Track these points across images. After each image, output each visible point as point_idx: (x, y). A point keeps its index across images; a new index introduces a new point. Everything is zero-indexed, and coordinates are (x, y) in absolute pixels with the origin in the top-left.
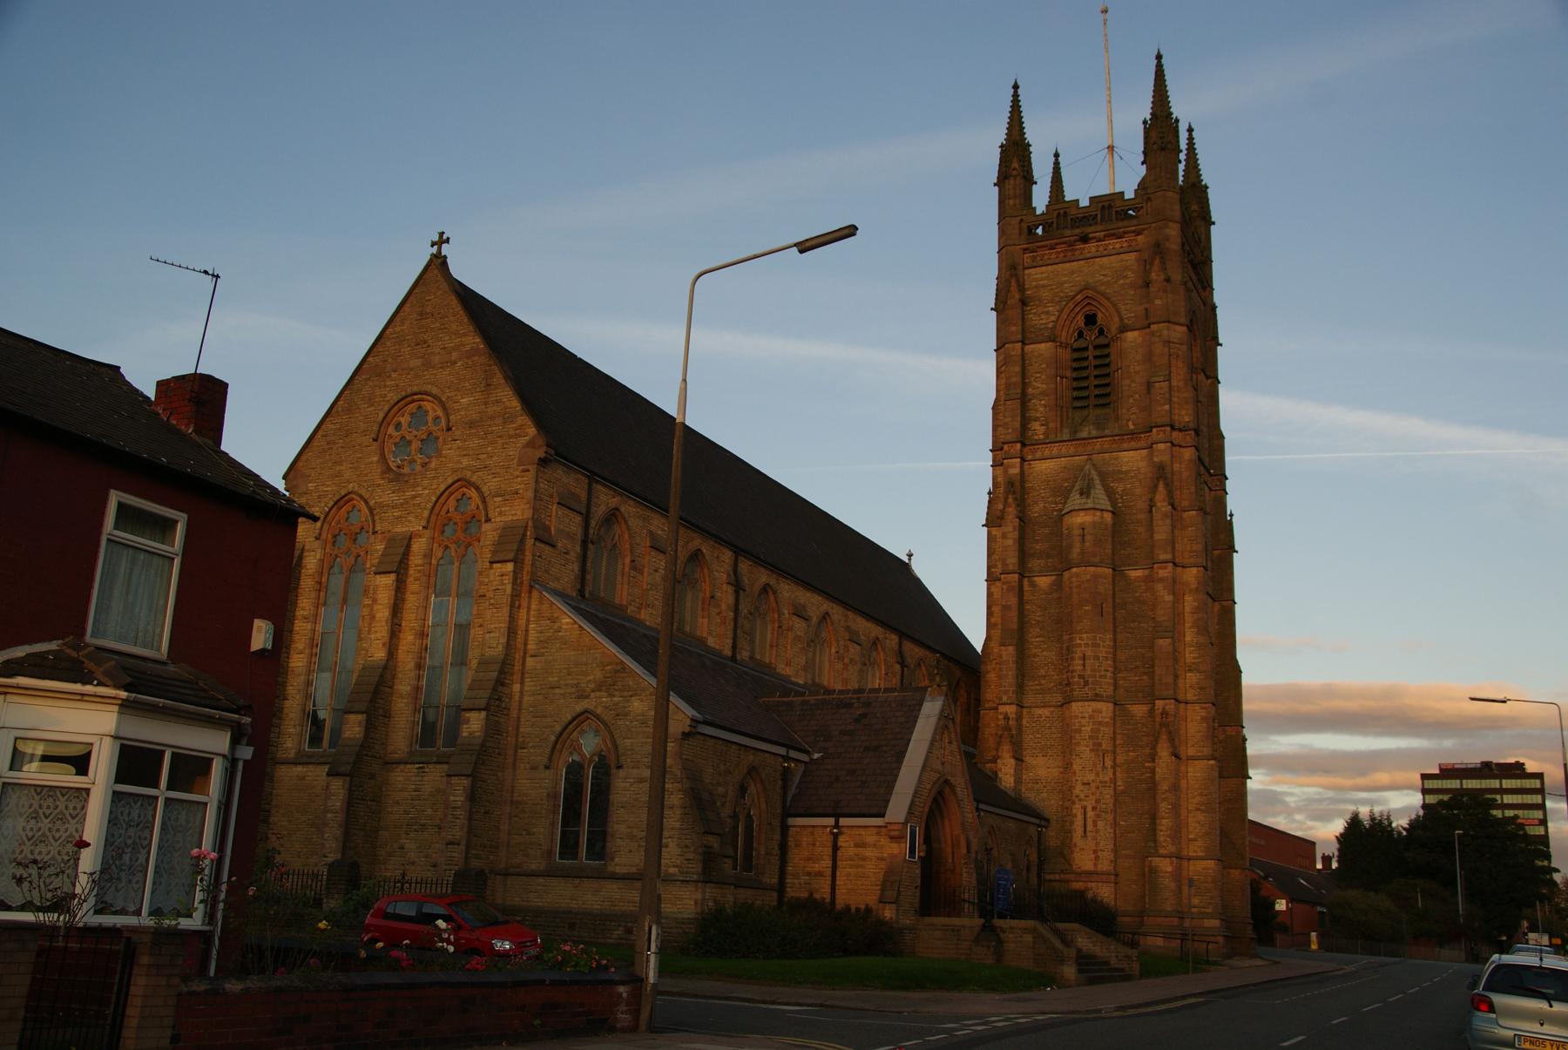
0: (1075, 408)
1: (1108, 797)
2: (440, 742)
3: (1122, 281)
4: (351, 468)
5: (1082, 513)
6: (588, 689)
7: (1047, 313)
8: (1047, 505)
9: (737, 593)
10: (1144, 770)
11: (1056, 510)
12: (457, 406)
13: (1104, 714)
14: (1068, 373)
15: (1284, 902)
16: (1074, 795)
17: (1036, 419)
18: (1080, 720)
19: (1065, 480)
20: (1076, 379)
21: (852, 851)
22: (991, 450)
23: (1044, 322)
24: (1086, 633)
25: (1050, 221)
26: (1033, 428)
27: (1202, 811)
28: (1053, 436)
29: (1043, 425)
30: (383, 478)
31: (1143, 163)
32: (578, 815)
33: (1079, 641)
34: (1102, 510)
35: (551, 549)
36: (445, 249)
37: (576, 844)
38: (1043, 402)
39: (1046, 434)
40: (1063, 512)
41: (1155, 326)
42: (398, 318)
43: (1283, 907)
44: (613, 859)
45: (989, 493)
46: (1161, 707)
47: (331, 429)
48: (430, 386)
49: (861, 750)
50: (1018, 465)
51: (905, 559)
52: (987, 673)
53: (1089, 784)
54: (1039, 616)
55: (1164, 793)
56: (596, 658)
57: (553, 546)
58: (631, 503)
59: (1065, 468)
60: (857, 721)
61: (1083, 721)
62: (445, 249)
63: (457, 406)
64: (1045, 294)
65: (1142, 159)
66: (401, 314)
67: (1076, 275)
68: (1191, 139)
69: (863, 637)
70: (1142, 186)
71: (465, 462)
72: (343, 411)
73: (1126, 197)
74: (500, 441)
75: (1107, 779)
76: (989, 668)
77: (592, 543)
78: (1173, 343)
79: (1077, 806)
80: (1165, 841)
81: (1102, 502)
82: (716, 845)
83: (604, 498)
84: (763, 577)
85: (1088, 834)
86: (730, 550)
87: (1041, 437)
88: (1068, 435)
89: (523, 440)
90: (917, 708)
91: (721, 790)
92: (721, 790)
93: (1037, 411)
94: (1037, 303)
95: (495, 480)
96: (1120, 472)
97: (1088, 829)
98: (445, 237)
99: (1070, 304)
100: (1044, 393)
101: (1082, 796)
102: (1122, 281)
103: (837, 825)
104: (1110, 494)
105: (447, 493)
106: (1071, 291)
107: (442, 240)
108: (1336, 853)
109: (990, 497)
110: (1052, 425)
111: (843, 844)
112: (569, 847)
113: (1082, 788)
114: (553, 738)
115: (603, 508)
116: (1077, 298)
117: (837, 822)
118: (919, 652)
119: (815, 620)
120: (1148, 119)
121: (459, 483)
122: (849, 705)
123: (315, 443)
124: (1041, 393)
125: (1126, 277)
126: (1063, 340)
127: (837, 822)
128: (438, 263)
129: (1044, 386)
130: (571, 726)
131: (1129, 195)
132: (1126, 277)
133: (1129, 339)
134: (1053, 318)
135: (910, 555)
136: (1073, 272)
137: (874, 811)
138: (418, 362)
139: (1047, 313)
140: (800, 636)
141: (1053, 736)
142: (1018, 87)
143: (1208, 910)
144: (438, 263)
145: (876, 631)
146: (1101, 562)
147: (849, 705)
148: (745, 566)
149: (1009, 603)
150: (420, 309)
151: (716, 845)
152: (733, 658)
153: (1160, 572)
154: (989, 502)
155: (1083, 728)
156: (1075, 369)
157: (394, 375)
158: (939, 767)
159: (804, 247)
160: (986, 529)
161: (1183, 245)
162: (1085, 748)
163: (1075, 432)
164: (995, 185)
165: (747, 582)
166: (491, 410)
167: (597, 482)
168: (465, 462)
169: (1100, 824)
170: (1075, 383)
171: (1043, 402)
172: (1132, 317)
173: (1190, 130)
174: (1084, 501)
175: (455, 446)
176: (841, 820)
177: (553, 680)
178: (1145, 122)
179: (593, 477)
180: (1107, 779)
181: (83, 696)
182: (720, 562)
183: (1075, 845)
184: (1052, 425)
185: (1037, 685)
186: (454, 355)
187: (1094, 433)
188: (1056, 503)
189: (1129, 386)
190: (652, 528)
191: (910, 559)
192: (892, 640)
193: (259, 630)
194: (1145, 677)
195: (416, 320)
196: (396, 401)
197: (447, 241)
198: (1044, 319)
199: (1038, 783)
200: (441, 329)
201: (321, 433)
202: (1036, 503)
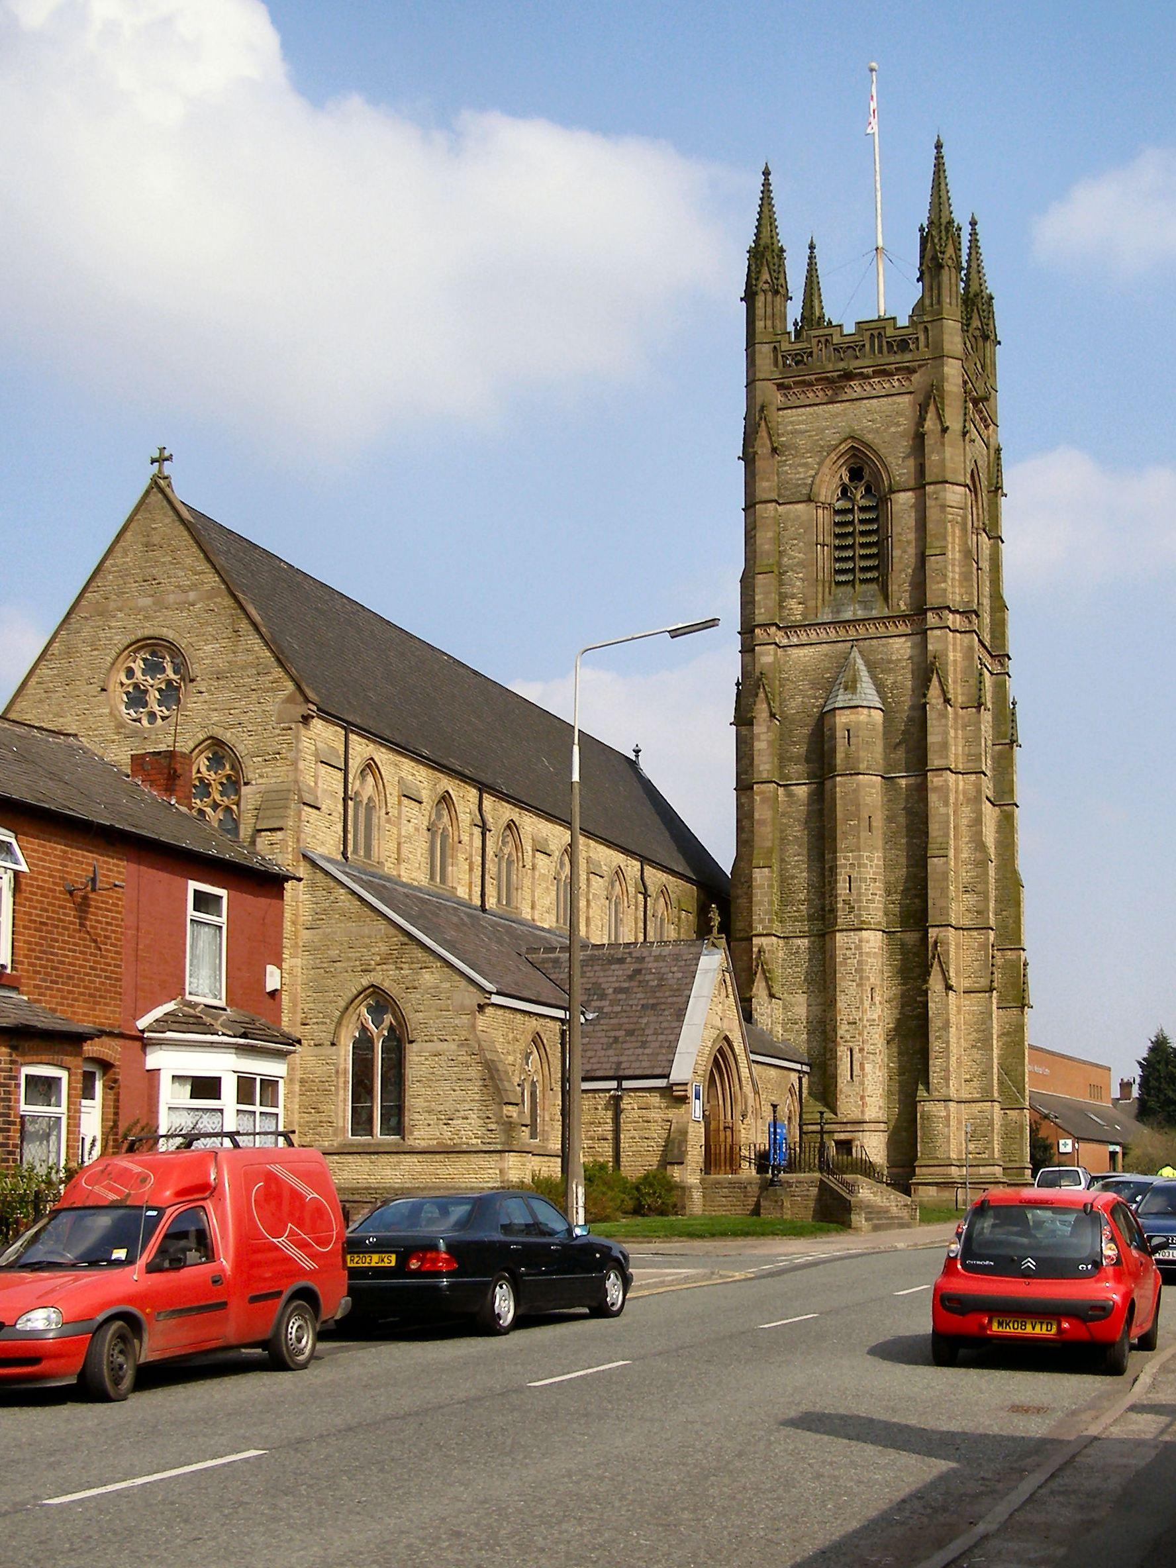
0: (838, 583)
1: (877, 1036)
2: (219, 1022)
3: (893, 429)
4: (77, 721)
5: (847, 712)
6: (373, 962)
7: (805, 465)
8: (806, 700)
9: (483, 834)
10: (916, 1005)
11: (817, 707)
12: (201, 654)
13: (872, 944)
14: (828, 540)
15: (1069, 1142)
16: (839, 1036)
17: (793, 596)
18: (845, 951)
19: (827, 670)
20: (837, 548)
21: (635, 1114)
22: (739, 633)
23: (802, 476)
24: (852, 851)
25: (809, 350)
26: (789, 607)
27: (979, 1049)
28: (813, 616)
29: (800, 603)
30: (119, 733)
31: (918, 280)
32: (370, 1091)
33: (843, 861)
34: (870, 707)
35: (317, 812)
36: (168, 468)
37: (370, 1120)
38: (801, 575)
39: (804, 615)
40: (825, 709)
41: (932, 487)
42: (118, 548)
43: (1069, 1149)
44: (411, 1133)
45: (738, 684)
46: (934, 935)
47: (48, 676)
48: (165, 629)
49: (639, 1008)
50: (772, 652)
51: (632, 756)
52: (738, 897)
53: (855, 1023)
54: (796, 831)
55: (937, 1031)
56: (380, 930)
57: (318, 809)
58: (383, 750)
59: (826, 655)
60: (631, 978)
61: (848, 952)
62: (168, 468)
63: (201, 654)
64: (801, 442)
65: (918, 275)
66: (122, 544)
67: (838, 419)
68: (974, 234)
69: (604, 868)
70: (919, 309)
71: (215, 717)
72: (60, 654)
73: (899, 324)
74: (254, 695)
75: (875, 1016)
76: (739, 892)
77: (351, 799)
78: (952, 507)
79: (842, 1048)
80: (939, 1083)
81: (870, 697)
82: (515, 1115)
83: (358, 748)
84: (508, 812)
85: (854, 1078)
86: (474, 787)
87: (799, 617)
88: (830, 616)
89: (282, 695)
90: (694, 962)
91: (511, 1058)
92: (511, 1058)
93: (793, 586)
94: (793, 452)
95: (252, 738)
96: (890, 661)
97: (855, 1074)
98: (166, 453)
99: (833, 455)
100: (801, 564)
101: (848, 1037)
102: (893, 429)
103: (619, 1088)
104: (880, 687)
105: (197, 750)
106: (834, 440)
107: (161, 459)
108: (1138, 1080)
109: (738, 689)
110: (812, 603)
111: (625, 1106)
112: (362, 1122)
113: (847, 1027)
114: (338, 1014)
115: (359, 760)
116: (841, 447)
117: (620, 1085)
118: (663, 877)
119: (557, 854)
120: (925, 226)
121: (209, 742)
122: (621, 961)
123: (29, 690)
124: (798, 564)
125: (898, 425)
126: (822, 499)
127: (620, 1085)
128: (159, 487)
129: (801, 555)
130: (356, 1001)
131: (903, 321)
132: (898, 425)
133: (901, 501)
134: (812, 472)
135: (637, 752)
136: (837, 415)
137: (658, 1071)
138: (148, 601)
139: (805, 465)
140: (544, 875)
141: (814, 969)
142: (769, 174)
143: (983, 1156)
144: (159, 487)
145: (618, 858)
146: (868, 768)
147: (621, 961)
148: (488, 801)
149: (762, 817)
150: (145, 539)
151: (515, 1115)
152: (483, 909)
153: (935, 779)
154: (737, 695)
155: (849, 961)
156: (837, 536)
157: (120, 615)
158: (719, 1024)
159: (675, 634)
160: (734, 727)
161: (965, 383)
162: (850, 983)
163: (838, 612)
164: (742, 299)
165: (491, 820)
166: (242, 658)
167: (353, 732)
168: (215, 717)
169: (868, 1067)
170: (837, 553)
171: (801, 575)
172: (904, 474)
173: (973, 223)
174: (850, 696)
175: (202, 699)
176: (624, 1082)
177: (334, 953)
178: (922, 229)
179: (349, 727)
180: (875, 1016)
181: (212, 1044)
182: (466, 798)
183: (841, 1091)
184: (812, 603)
185: (795, 911)
186: (192, 596)
187: (860, 614)
188: (816, 698)
189: (901, 557)
190: (403, 774)
191: (637, 756)
192: (632, 867)
193: (272, 974)
194: (916, 901)
195: (141, 552)
196: (126, 644)
197: (169, 458)
198: (802, 473)
199: (797, 1023)
200: (172, 564)
201: (34, 680)
202: (792, 697)
